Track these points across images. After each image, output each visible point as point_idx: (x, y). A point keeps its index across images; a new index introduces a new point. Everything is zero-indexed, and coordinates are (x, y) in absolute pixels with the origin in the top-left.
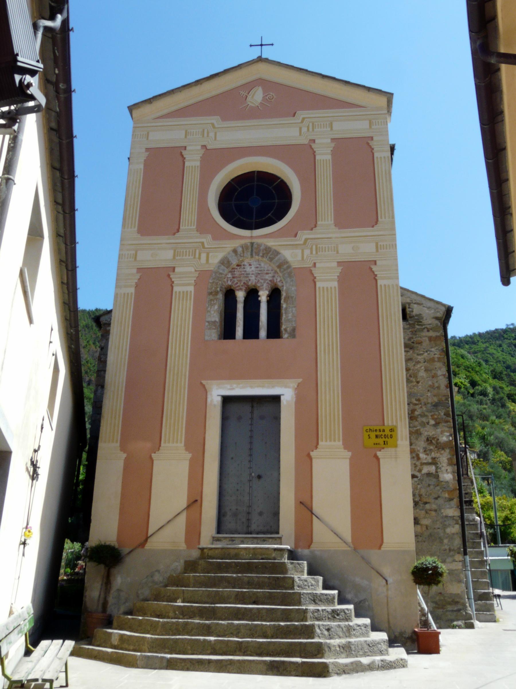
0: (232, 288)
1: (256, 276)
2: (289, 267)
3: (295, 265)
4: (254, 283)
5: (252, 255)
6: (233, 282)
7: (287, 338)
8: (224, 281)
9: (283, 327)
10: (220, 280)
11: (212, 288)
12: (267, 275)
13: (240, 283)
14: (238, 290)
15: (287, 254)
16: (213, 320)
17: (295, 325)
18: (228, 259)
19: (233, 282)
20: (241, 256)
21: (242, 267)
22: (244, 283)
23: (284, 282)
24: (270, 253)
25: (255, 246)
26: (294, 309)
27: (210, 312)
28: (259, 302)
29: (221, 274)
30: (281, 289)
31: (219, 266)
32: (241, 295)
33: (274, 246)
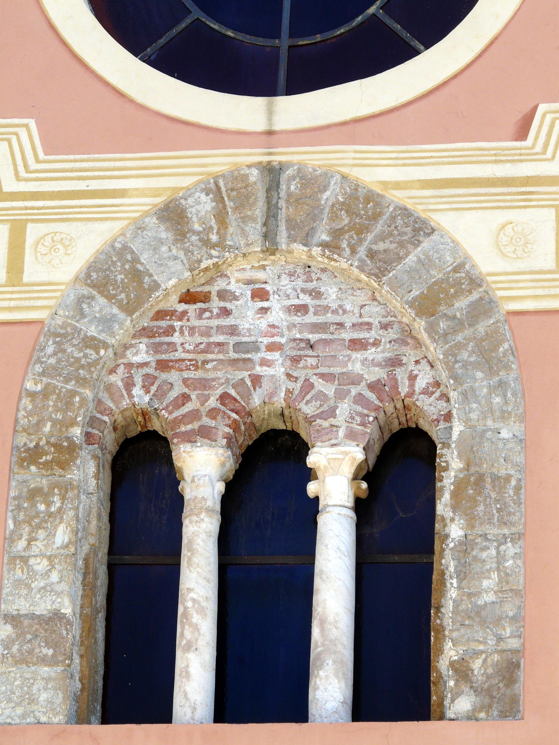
0: (156, 425)
1: (295, 360)
2: (484, 307)
3: (515, 297)
4: (280, 401)
5: (269, 236)
6: (160, 395)
7: (471, 717)
8: (109, 388)
9: (447, 655)
10: (82, 382)
11: (39, 425)
12: (358, 355)
13: (204, 400)
14: (189, 438)
15: (475, 234)
16: (43, 607)
17: (514, 643)
18: (136, 260)
19: (160, 395)
20: (207, 243)
21: (216, 304)
22: (224, 398)
23: (453, 395)
24: (374, 230)
25: (289, 186)
26: (510, 549)
27: (25, 560)
28: (313, 507)
29: (92, 343)
30: (436, 433)
31: (81, 300)
32: (203, 470)
33: (398, 185)
